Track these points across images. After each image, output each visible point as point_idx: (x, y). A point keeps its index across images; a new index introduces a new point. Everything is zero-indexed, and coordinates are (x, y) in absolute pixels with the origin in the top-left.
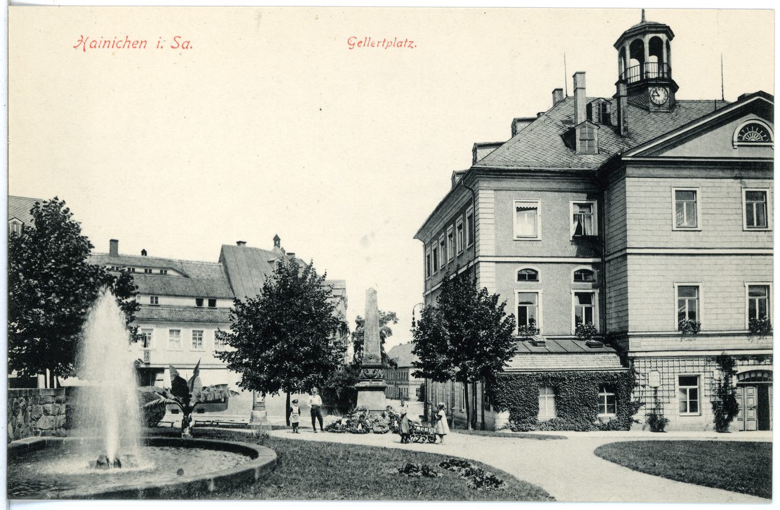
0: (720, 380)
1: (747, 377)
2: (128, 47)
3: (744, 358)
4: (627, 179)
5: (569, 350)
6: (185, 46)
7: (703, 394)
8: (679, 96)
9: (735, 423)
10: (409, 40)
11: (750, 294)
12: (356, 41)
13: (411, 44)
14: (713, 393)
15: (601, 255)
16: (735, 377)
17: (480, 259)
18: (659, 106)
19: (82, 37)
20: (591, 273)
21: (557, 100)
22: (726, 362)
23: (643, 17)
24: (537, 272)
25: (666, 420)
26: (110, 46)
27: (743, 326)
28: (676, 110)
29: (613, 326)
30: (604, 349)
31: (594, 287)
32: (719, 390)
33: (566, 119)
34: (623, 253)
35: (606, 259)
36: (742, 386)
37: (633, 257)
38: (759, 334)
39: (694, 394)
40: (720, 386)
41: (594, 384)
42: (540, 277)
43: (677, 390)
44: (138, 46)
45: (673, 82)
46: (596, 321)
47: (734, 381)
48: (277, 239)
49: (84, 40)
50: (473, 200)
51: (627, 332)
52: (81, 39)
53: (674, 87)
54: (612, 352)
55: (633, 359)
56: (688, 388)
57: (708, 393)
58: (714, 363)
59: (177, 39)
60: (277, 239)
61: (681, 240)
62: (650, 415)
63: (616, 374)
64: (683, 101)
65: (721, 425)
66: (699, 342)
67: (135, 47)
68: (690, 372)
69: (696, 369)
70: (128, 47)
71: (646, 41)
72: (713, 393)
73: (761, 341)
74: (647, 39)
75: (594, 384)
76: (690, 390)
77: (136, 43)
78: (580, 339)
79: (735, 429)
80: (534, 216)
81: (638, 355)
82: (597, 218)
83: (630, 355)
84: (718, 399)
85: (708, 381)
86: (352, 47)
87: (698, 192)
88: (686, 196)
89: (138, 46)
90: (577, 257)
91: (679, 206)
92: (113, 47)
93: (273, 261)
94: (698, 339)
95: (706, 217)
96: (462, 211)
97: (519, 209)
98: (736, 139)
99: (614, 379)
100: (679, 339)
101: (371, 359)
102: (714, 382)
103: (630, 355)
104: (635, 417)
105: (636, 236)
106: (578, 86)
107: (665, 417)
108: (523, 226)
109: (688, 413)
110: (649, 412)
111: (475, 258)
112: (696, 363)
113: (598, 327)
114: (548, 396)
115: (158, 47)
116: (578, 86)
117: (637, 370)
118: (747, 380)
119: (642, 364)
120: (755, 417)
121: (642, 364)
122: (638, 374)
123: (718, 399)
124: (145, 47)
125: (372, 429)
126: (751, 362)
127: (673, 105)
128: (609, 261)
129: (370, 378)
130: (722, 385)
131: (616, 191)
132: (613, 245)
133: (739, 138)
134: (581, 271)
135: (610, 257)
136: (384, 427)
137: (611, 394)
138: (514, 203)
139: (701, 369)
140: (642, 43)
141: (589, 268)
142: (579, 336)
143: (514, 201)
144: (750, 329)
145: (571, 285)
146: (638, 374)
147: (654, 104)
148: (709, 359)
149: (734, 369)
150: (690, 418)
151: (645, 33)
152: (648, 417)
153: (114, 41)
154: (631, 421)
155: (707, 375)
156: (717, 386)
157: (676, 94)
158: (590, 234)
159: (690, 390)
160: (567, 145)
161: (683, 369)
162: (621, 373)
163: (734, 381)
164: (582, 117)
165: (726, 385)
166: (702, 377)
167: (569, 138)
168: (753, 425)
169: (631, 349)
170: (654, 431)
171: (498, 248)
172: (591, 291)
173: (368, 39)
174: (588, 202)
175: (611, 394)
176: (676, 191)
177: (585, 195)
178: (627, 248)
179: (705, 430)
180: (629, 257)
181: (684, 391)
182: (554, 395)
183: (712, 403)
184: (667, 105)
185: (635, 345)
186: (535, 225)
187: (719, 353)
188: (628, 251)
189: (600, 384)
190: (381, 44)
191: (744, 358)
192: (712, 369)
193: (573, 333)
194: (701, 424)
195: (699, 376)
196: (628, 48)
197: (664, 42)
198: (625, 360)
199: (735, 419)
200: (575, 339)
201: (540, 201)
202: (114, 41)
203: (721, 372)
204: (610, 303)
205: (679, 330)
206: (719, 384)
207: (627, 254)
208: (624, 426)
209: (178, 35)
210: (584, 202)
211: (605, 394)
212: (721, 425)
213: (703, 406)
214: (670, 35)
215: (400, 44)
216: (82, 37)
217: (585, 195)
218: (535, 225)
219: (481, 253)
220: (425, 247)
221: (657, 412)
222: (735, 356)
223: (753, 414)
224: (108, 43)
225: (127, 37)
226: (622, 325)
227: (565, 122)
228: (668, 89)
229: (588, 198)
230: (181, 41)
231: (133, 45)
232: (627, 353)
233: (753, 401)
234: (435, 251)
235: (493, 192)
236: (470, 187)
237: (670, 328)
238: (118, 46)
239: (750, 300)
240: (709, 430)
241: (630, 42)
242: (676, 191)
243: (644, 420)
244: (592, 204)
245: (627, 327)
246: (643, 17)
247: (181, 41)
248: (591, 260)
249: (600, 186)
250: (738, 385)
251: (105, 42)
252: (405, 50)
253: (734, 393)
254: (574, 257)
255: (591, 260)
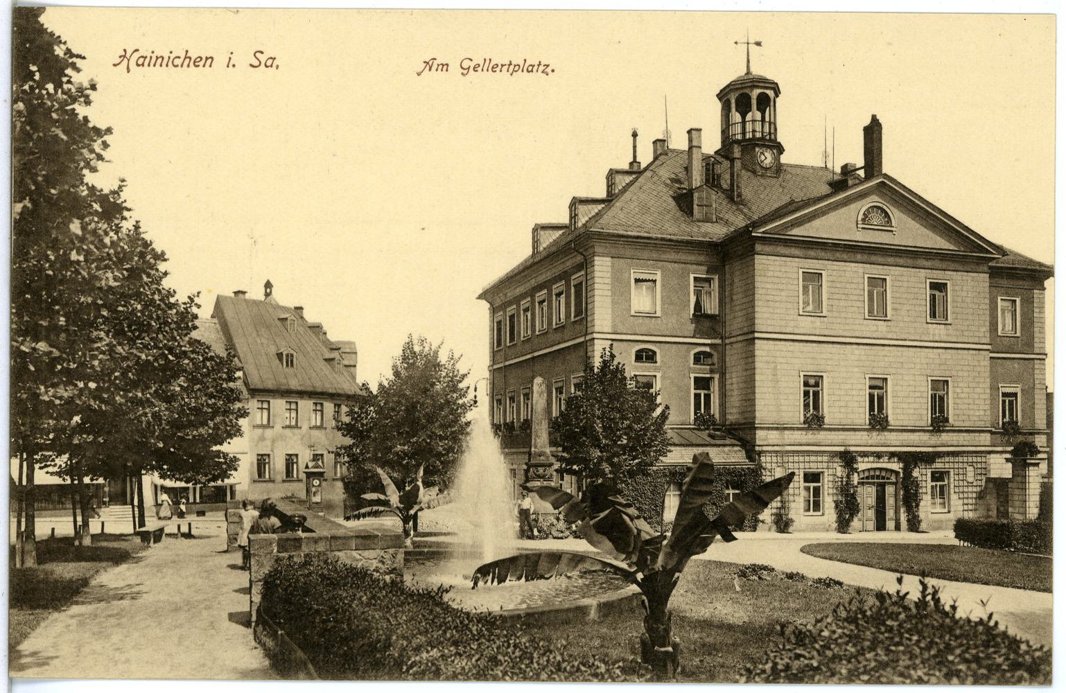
0: (842, 478)
1: (867, 474)
2: (188, 66)
3: (865, 454)
4: (756, 256)
5: (694, 442)
6: (269, 63)
8: (784, 159)
9: (856, 523)
10: (543, 63)
11: (871, 387)
12: (472, 64)
13: (546, 69)
15: (724, 336)
16: (856, 475)
17: (595, 336)
18: (766, 169)
19: (125, 51)
20: (709, 355)
22: (848, 459)
23: (748, 67)
24: (654, 353)
25: (792, 521)
26: (164, 64)
27: (863, 421)
28: (782, 175)
29: (733, 416)
30: (728, 441)
32: (841, 488)
33: (673, 176)
34: (751, 336)
35: (727, 341)
36: (863, 484)
37: (762, 342)
38: (878, 430)
39: (817, 491)
40: (842, 484)
41: (721, 480)
42: (658, 358)
43: (802, 488)
44: (201, 64)
45: (779, 143)
47: (855, 479)
49: (128, 56)
50: (585, 265)
51: (754, 423)
52: (124, 54)
53: (780, 149)
54: (737, 445)
55: (759, 454)
56: (812, 485)
57: (831, 491)
58: (837, 459)
59: (258, 55)
61: (807, 325)
62: (776, 514)
63: (743, 469)
64: (791, 166)
65: (843, 526)
66: (822, 436)
67: (199, 66)
68: (814, 468)
69: (820, 465)
70: (188, 66)
71: (748, 97)
73: (879, 437)
74: (756, 92)
75: (721, 480)
76: (814, 488)
77: (199, 59)
78: (699, 429)
79: (854, 530)
80: (653, 290)
81: (765, 448)
82: (717, 295)
83: (757, 448)
85: (831, 478)
86: (465, 72)
88: (813, 278)
89: (201, 64)
90: (693, 337)
91: (805, 288)
92: (167, 66)
93: (286, 319)
94: (822, 433)
97: (637, 281)
99: (741, 475)
100: (804, 433)
101: (540, 456)
102: (837, 480)
103: (757, 448)
104: (761, 517)
105: (765, 318)
106: (695, 143)
107: (790, 516)
108: (641, 301)
109: (811, 512)
112: (820, 459)
113: (717, 416)
114: (674, 493)
115: (228, 66)
116: (695, 143)
117: (764, 465)
119: (768, 459)
120: (874, 518)
121: (768, 459)
122: (764, 469)
124: (210, 66)
125: (551, 534)
126: (871, 459)
127: (779, 169)
128: (731, 343)
129: (541, 478)
130: (844, 483)
132: (735, 324)
135: (733, 340)
136: (562, 532)
137: (737, 492)
139: (825, 465)
140: (750, 98)
141: (707, 349)
142: (699, 425)
143: (632, 271)
144: (870, 424)
145: (690, 368)
146: (764, 469)
147: (762, 167)
148: (834, 454)
149: (855, 466)
150: (814, 519)
152: (773, 518)
153: (169, 57)
154: (757, 521)
155: (831, 471)
156: (840, 483)
157: (782, 156)
158: (709, 312)
159: (814, 488)
160: (681, 209)
161: (807, 465)
162: (748, 468)
163: (855, 479)
164: (697, 178)
165: (847, 484)
166: (826, 474)
167: (684, 201)
168: (871, 525)
169: (758, 442)
170: (781, 532)
171: (614, 326)
172: (708, 376)
173: (488, 61)
175: (737, 492)
176: (803, 272)
179: (828, 531)
180: (756, 341)
181: (808, 489)
182: (679, 493)
183: (835, 501)
184: (774, 169)
185: (763, 438)
186: (654, 298)
187: (842, 449)
188: (757, 335)
190: (505, 68)
191: (865, 454)
192: (835, 465)
194: (824, 524)
195: (822, 472)
196: (733, 101)
199: (856, 519)
200: (694, 429)
201: (659, 273)
202: (169, 57)
203: (843, 469)
204: (732, 390)
205: (804, 423)
206: (842, 481)
207: (754, 339)
208: (750, 527)
210: (704, 276)
211: (731, 492)
212: (843, 526)
213: (827, 505)
215: (530, 68)
216: (125, 51)
217: (704, 268)
218: (654, 298)
219: (596, 329)
221: (782, 511)
222: (856, 452)
223: (871, 514)
224: (160, 60)
225: (187, 51)
226: (747, 415)
227: (672, 180)
228: (775, 151)
229: (708, 272)
230: (263, 58)
231: (195, 62)
232: (754, 446)
233: (872, 501)
235: (609, 259)
236: (581, 251)
237: (795, 420)
238: (175, 64)
239: (870, 394)
240: (832, 531)
242: (803, 272)
243: (770, 520)
244: (713, 279)
245: (755, 417)
246: (748, 67)
247: (263, 58)
248: (709, 341)
249: (730, 256)
250: (859, 483)
251: (157, 58)
252: (537, 76)
253: (855, 492)
254: (690, 337)
255: (709, 341)
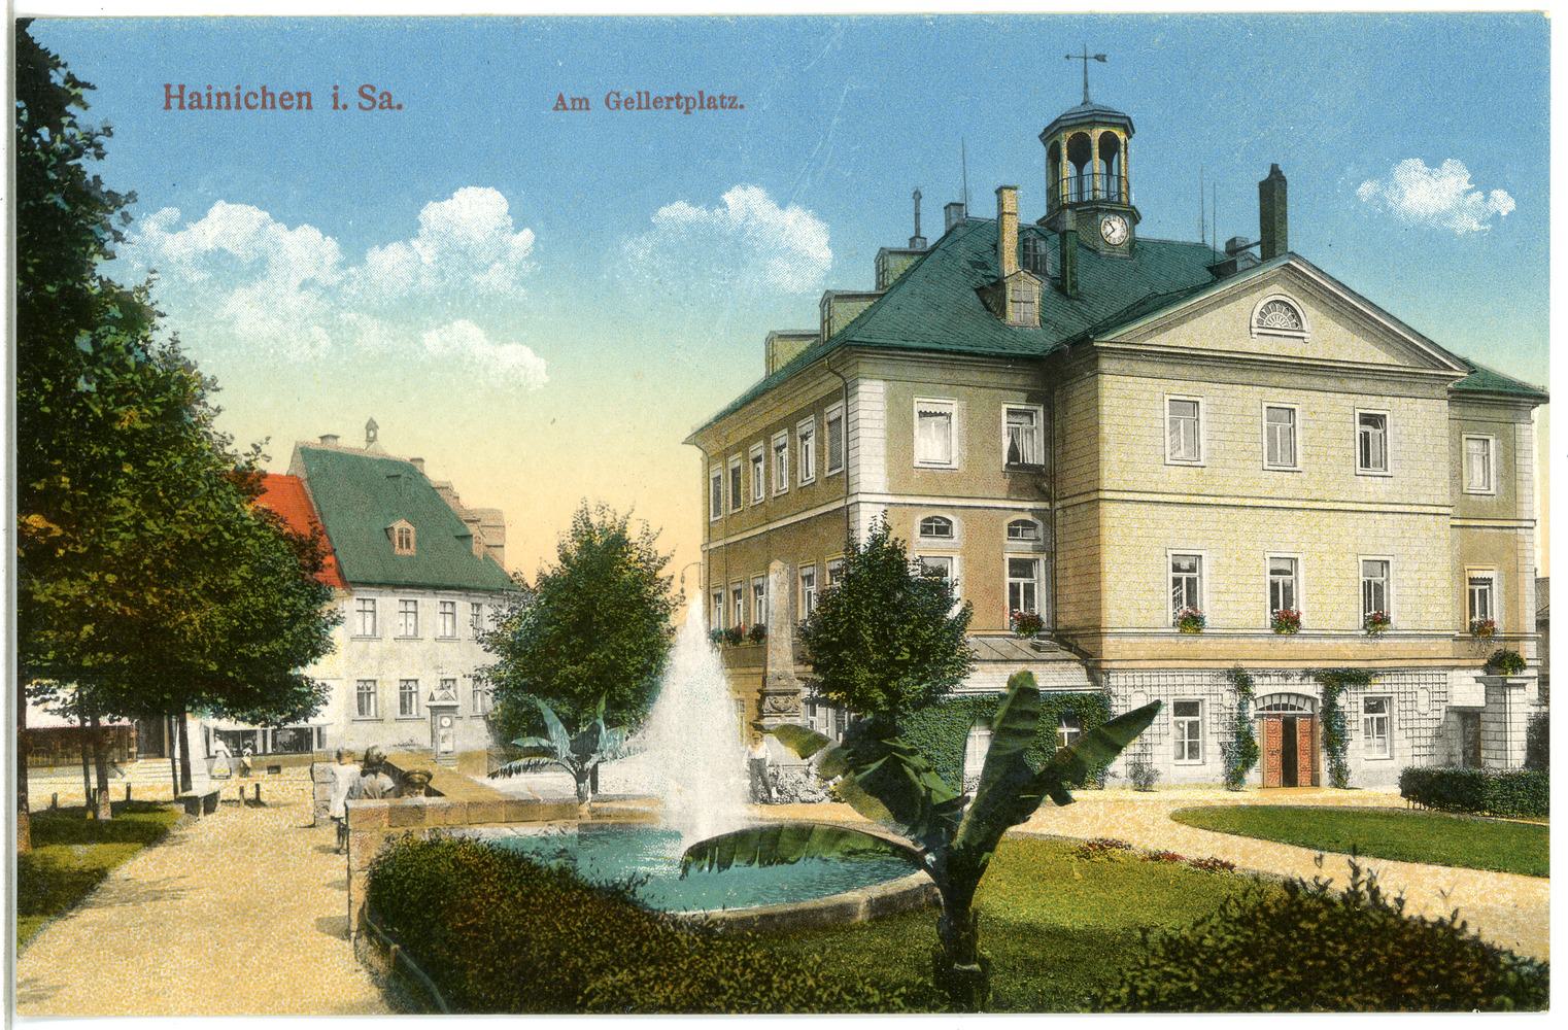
1: (1268, 702)
3: (1265, 674)
7: (1208, 730)
9: (1253, 776)
14: (1221, 728)
20: (1033, 526)
21: (953, 223)
24: (950, 522)
29: (1070, 617)
31: (1038, 550)
39: (1194, 729)
41: (1051, 713)
43: (1172, 725)
46: (1041, 608)
48: (371, 426)
50: (845, 392)
58: (1223, 680)
60: (371, 426)
61: (1176, 479)
65: (1235, 780)
69: (1199, 690)
72: (1221, 728)
74: (1096, 134)
75: (1051, 713)
81: (1115, 665)
84: (1229, 739)
87: (1201, 406)
88: (1186, 408)
95: (1214, 445)
96: (818, 408)
98: (1254, 324)
105: (1115, 471)
107: (1154, 767)
109: (1186, 760)
110: (1131, 758)
111: (848, 495)
117: (1113, 689)
118: (1269, 708)
119: (1122, 681)
121: (1122, 681)
123: (1229, 739)
126: (1274, 679)
131: (1078, 392)
133: (1258, 321)
134: (1016, 523)
138: (915, 405)
141: (1029, 517)
150: (1190, 770)
151: (1093, 124)
166: (1207, 703)
172: (1030, 557)
173: (644, 96)
174: (1029, 408)
177: (1024, 395)
178: (1098, 490)
185: (1110, 647)
187: (1230, 665)
189: (1059, 713)
192: (1221, 689)
193: (1007, 626)
195: (1202, 700)
197: (1122, 142)
198: (1095, 671)
200: (1011, 636)
203: (1232, 695)
209: (373, 83)
212: (1235, 780)
213: (1208, 749)
214: (1129, 129)
220: (708, 464)
221: (1143, 760)
234: (736, 471)
241: (1069, 135)
244: (1036, 411)
250: (1256, 716)
